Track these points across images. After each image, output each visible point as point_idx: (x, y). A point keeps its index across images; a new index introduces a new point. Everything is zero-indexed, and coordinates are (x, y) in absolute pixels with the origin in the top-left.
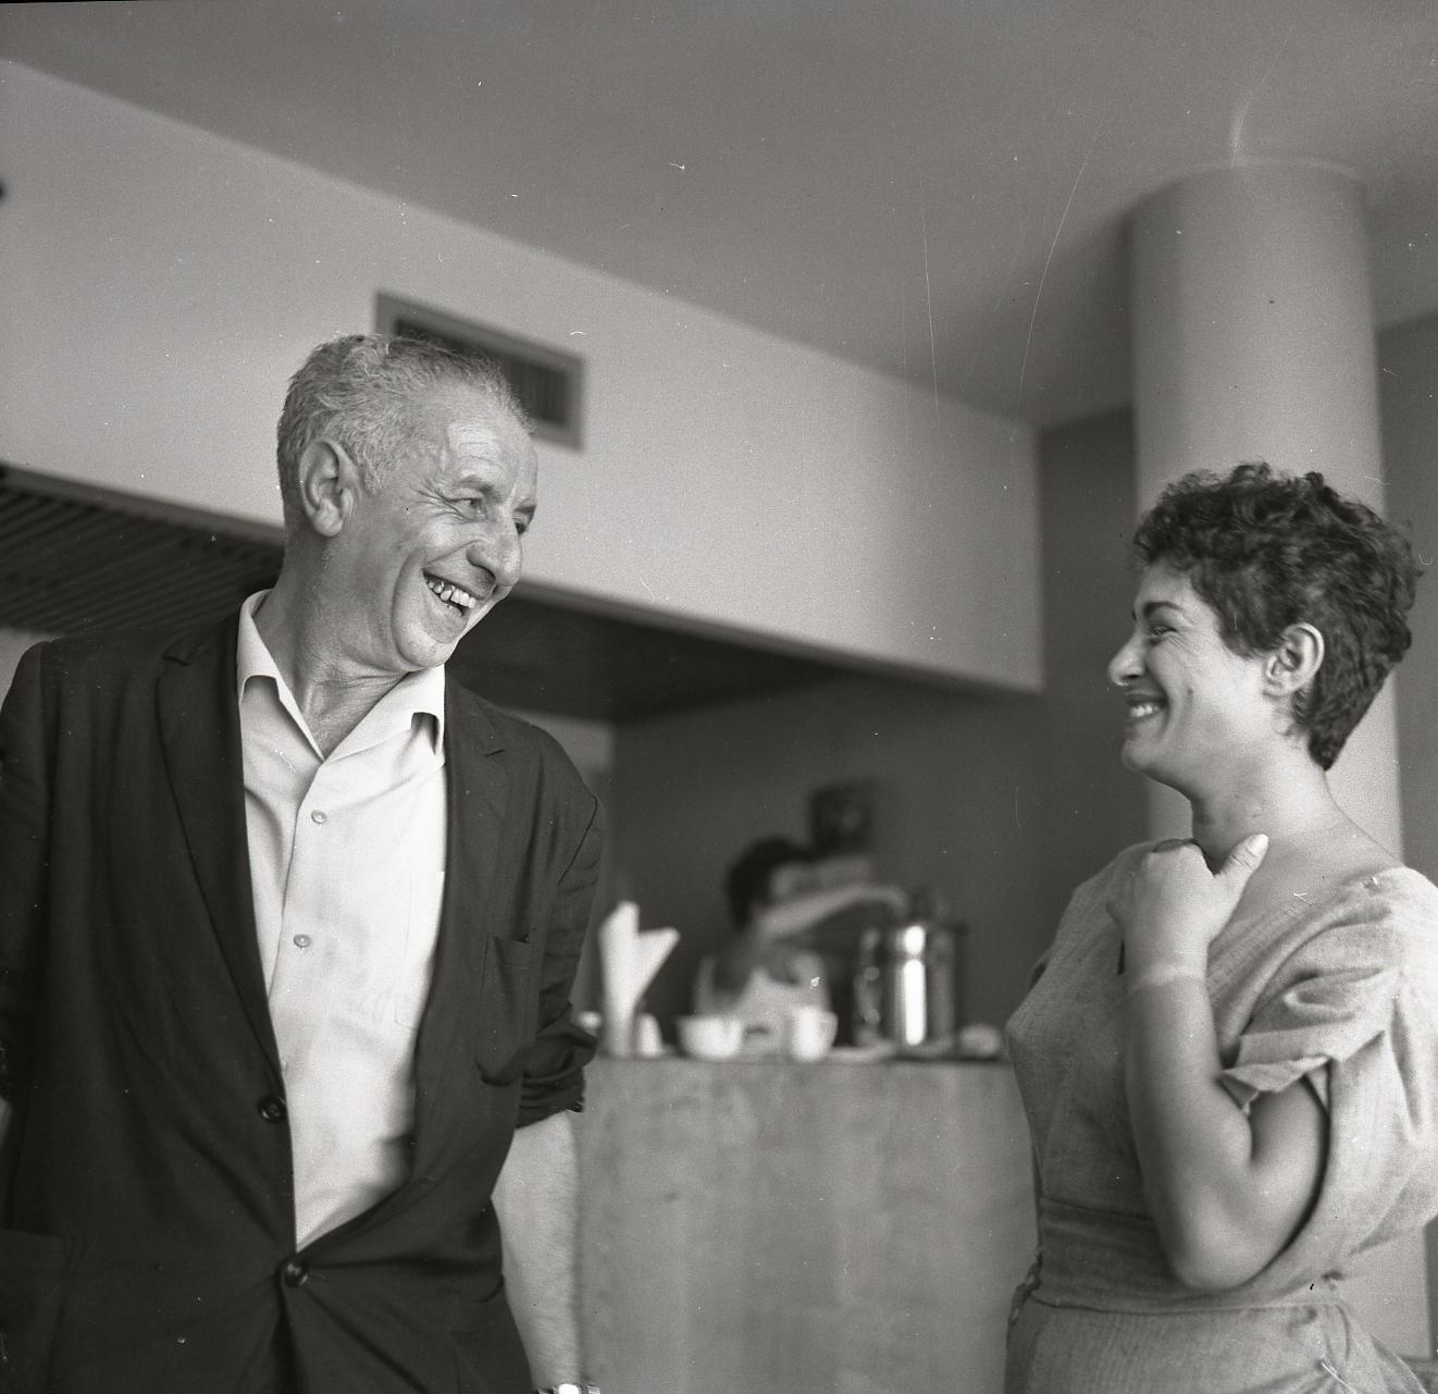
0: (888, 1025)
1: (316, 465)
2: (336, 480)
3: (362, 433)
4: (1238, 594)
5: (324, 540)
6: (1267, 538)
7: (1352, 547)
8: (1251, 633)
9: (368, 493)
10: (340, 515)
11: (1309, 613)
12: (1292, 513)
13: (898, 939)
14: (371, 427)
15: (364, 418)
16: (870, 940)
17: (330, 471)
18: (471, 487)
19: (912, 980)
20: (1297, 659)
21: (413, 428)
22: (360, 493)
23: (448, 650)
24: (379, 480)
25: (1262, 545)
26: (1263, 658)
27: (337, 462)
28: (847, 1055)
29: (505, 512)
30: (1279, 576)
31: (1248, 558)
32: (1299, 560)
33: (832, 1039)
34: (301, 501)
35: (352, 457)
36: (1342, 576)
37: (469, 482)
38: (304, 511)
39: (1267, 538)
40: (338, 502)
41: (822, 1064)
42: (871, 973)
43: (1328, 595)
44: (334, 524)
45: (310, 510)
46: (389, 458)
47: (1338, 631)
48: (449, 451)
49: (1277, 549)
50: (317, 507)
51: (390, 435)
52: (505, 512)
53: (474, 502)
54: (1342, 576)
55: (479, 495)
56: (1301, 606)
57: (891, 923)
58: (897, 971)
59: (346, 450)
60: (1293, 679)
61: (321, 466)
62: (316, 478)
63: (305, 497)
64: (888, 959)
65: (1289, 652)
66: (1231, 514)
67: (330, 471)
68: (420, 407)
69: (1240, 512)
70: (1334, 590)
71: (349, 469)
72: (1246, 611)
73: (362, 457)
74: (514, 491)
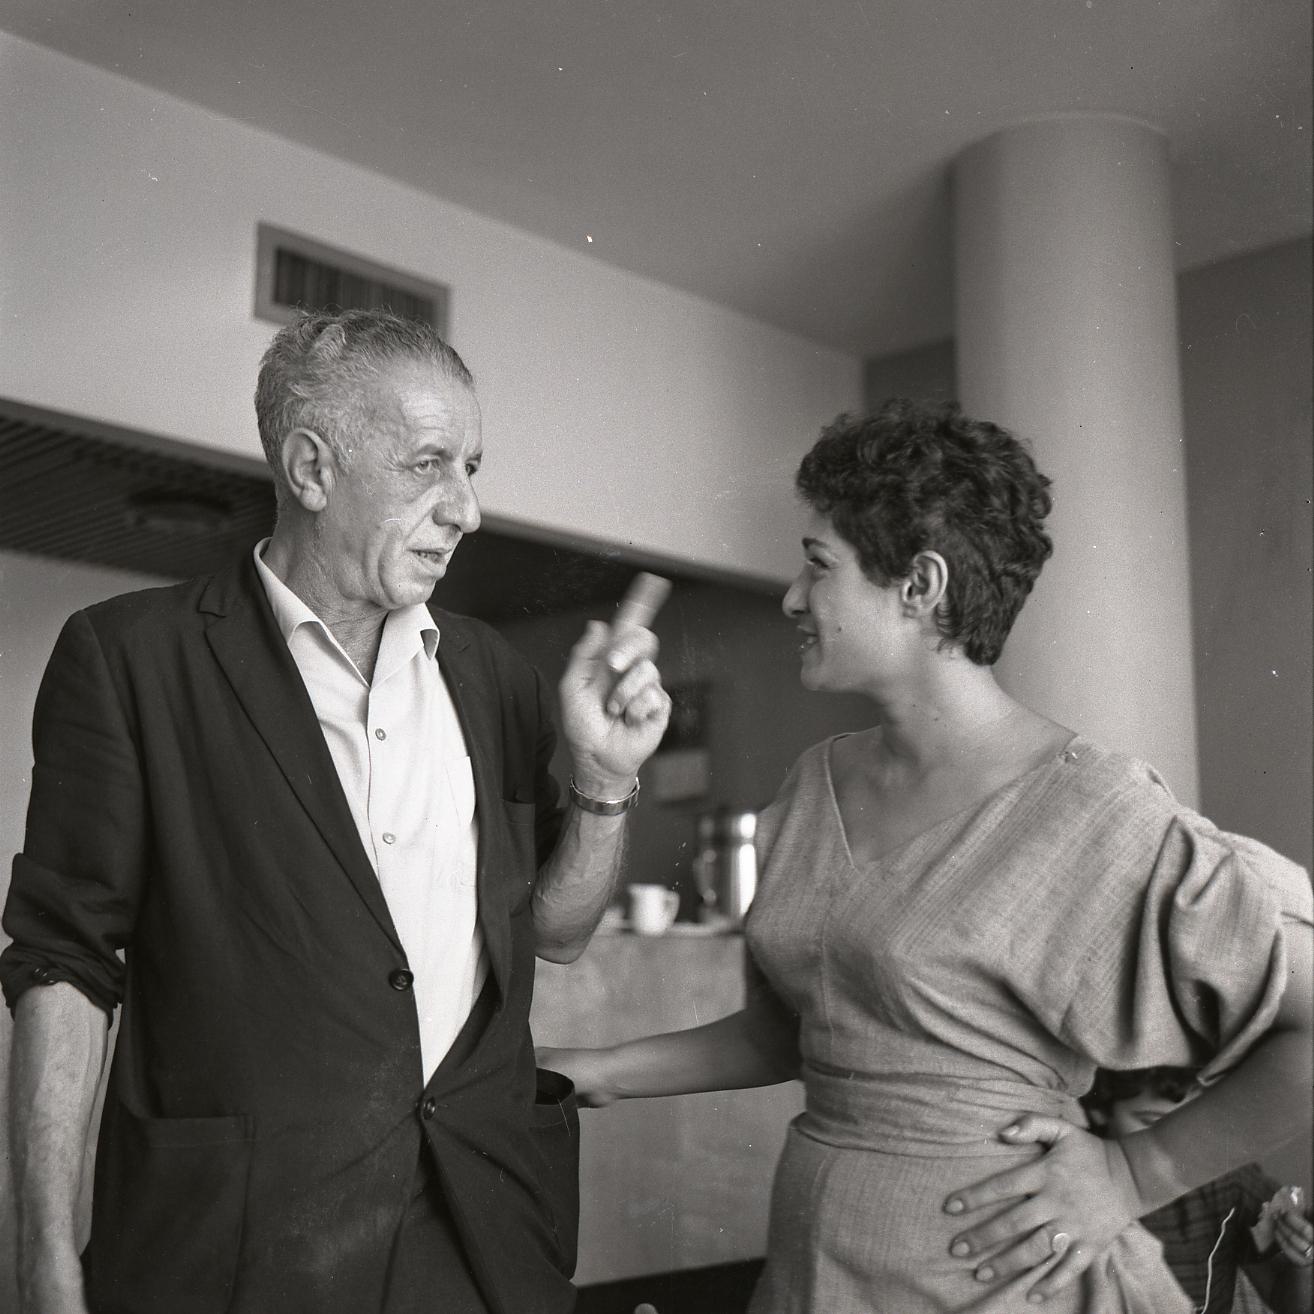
0: (724, 903)
1: (296, 451)
2: (315, 461)
3: (332, 420)
4: (870, 531)
5: (314, 515)
6: (890, 478)
7: (965, 475)
8: (887, 563)
9: (342, 472)
10: (324, 492)
11: (933, 540)
12: (909, 451)
13: (733, 824)
14: (340, 413)
15: (332, 407)
16: (707, 827)
17: (309, 455)
18: (426, 453)
19: (746, 861)
20: (924, 586)
21: (375, 411)
22: (336, 470)
23: (428, 590)
24: (349, 456)
25: (882, 486)
26: (898, 586)
27: (315, 447)
28: (688, 929)
29: (459, 465)
30: (901, 515)
31: (872, 498)
32: (918, 495)
33: (674, 915)
34: (287, 482)
35: (325, 440)
36: (958, 504)
37: (426, 449)
38: (290, 492)
39: (890, 478)
40: (320, 482)
41: (666, 938)
42: (709, 856)
43: (948, 522)
44: (320, 500)
45: (297, 490)
46: (357, 440)
47: (962, 551)
48: (405, 425)
49: (898, 489)
50: (303, 487)
51: (356, 420)
52: (459, 465)
53: (435, 462)
54: (958, 504)
55: (435, 457)
56: (923, 537)
57: (726, 813)
58: (733, 854)
59: (320, 436)
60: (925, 603)
61: (301, 453)
62: (298, 463)
63: (291, 483)
64: (725, 843)
65: (919, 575)
66: (856, 458)
67: (309, 455)
68: (379, 391)
69: (863, 455)
70: (954, 519)
71: (325, 453)
72: (876, 545)
73: (334, 440)
74: (464, 447)
